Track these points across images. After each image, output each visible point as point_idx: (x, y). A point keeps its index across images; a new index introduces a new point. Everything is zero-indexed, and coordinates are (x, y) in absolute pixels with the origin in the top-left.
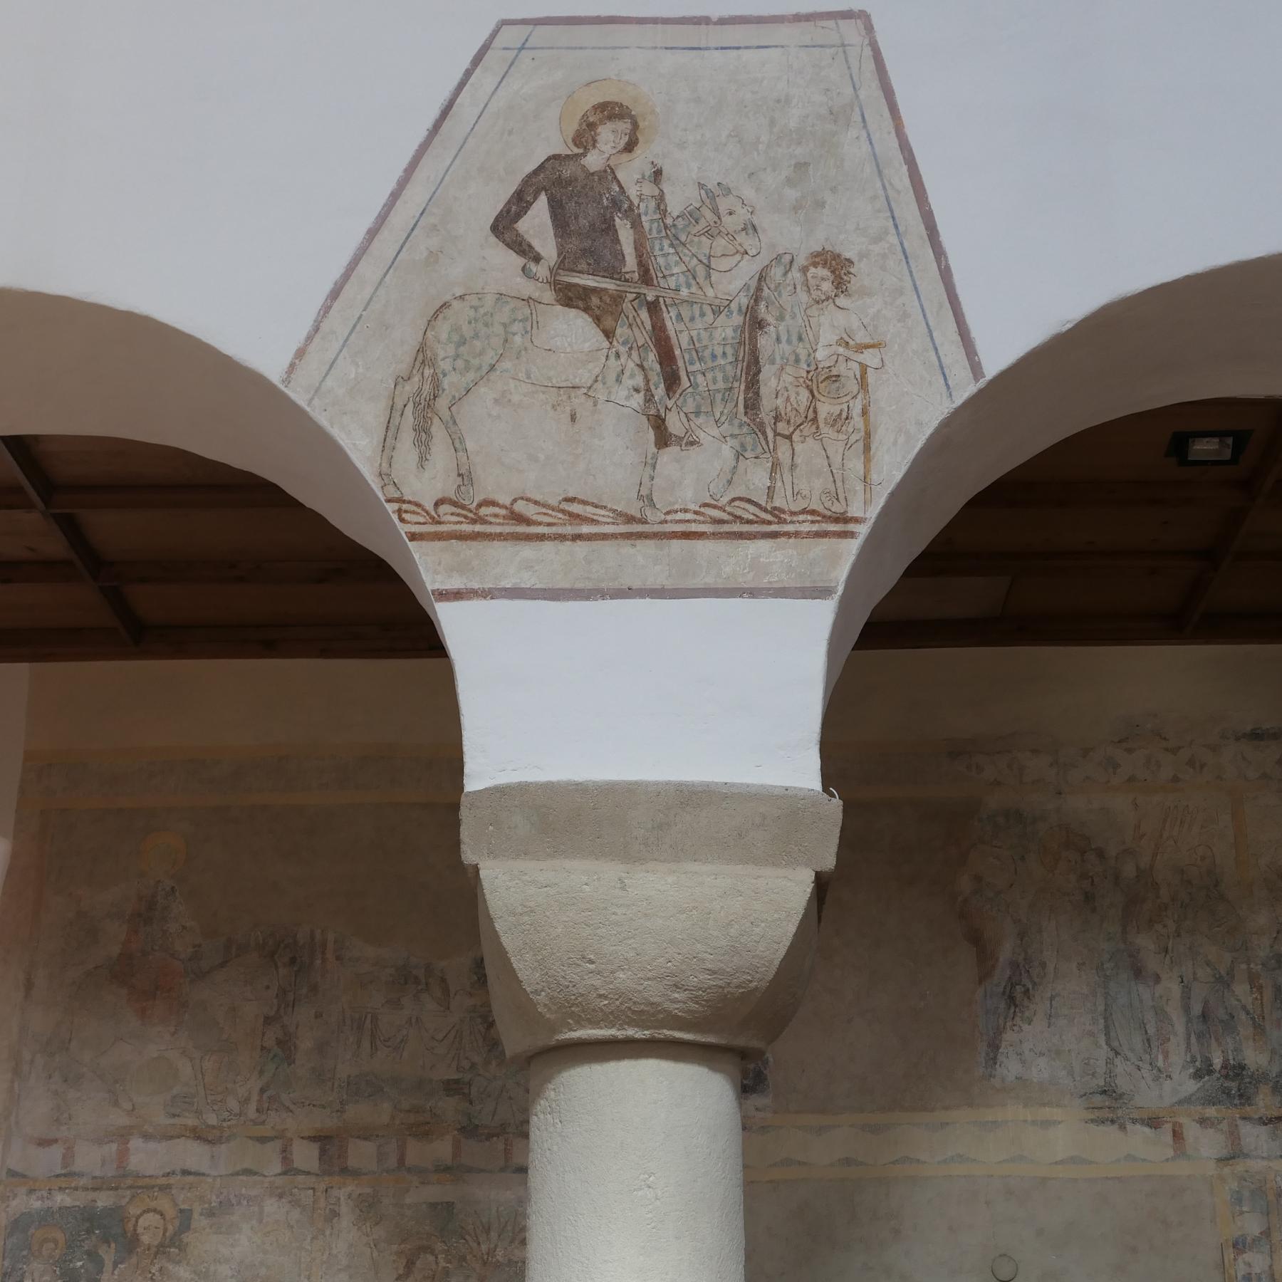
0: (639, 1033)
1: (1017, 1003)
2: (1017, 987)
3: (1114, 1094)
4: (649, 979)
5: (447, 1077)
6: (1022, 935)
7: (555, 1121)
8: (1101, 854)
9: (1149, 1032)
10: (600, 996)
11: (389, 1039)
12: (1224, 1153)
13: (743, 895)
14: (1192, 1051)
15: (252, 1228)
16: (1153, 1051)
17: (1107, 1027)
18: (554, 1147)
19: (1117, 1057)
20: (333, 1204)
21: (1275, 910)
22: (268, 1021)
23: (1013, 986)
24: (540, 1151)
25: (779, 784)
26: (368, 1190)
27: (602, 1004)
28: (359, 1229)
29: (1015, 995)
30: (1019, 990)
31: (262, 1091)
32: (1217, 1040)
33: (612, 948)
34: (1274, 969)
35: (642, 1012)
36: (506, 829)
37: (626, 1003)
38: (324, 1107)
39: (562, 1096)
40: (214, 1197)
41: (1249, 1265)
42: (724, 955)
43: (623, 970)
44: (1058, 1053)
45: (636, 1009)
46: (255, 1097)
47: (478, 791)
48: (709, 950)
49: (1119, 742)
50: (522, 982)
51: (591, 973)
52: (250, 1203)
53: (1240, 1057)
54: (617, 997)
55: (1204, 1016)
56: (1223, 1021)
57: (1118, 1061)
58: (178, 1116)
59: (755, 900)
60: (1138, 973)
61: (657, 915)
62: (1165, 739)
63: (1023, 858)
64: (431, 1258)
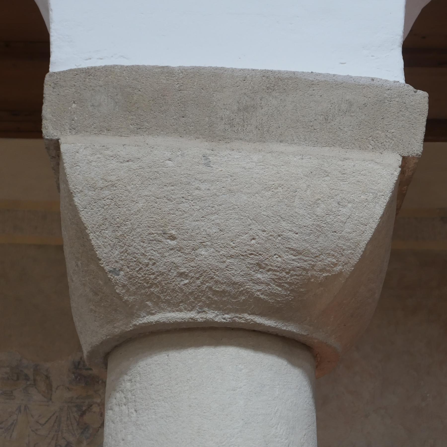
0: (220, 317)
4: (231, 256)
7: (130, 410)
10: (181, 275)
13: (329, 175)
18: (129, 436)
25: (364, 76)
27: (182, 283)
33: (194, 224)
35: (224, 292)
36: (89, 106)
37: (207, 282)
39: (138, 385)
42: (309, 234)
43: (205, 246)
45: (218, 289)
47: (63, 72)
48: (294, 229)
50: (100, 260)
51: (172, 249)
54: (197, 276)
59: (342, 180)
61: (242, 192)
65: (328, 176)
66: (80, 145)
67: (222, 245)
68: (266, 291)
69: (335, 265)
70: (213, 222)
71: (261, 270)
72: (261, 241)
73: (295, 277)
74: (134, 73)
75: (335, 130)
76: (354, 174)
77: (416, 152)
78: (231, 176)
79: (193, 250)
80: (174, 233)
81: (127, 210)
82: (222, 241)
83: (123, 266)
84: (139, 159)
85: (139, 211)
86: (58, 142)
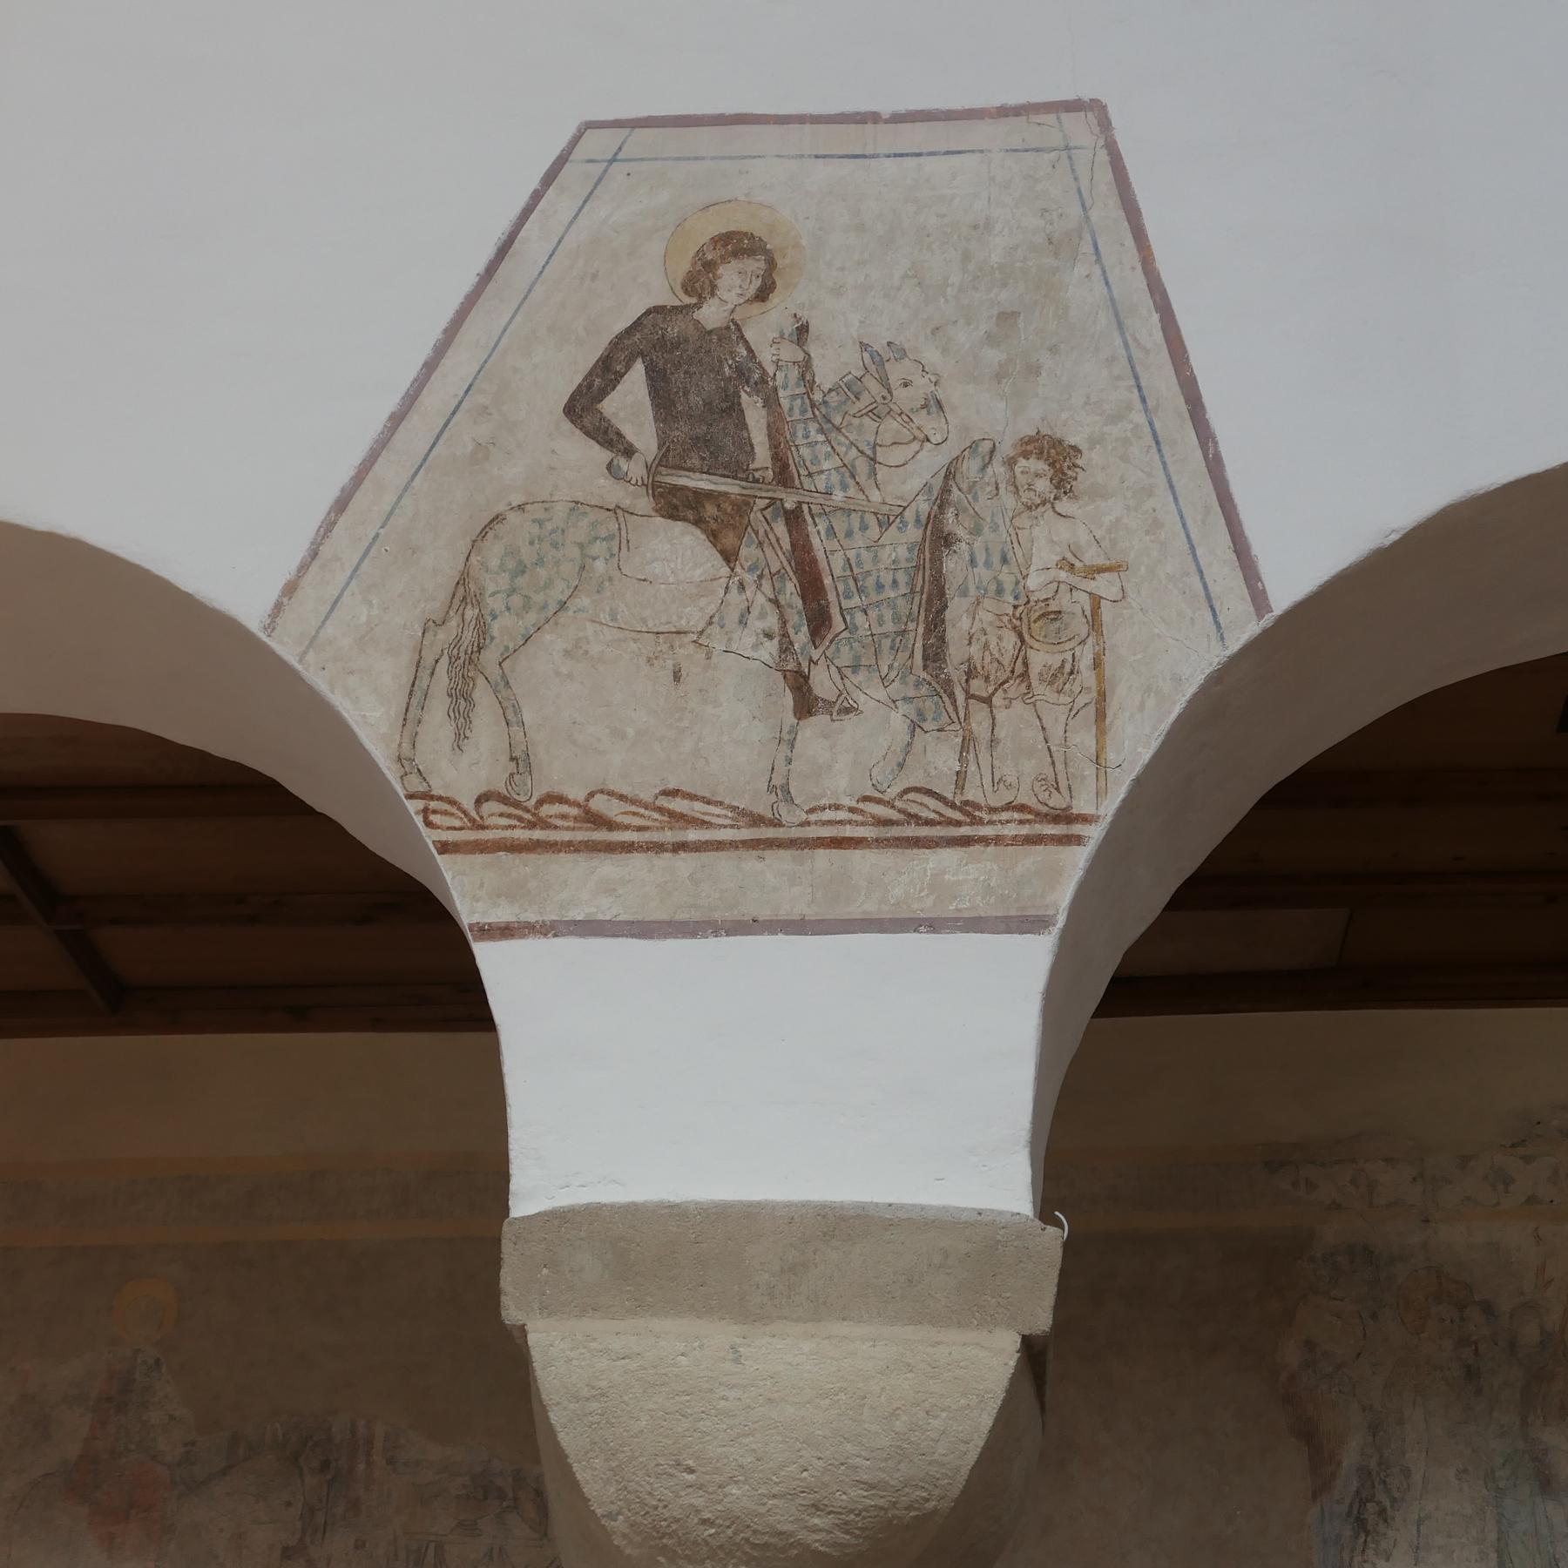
2: (1369, 1505)
4: (774, 1496)
8: (1488, 1309)
10: (704, 1522)
23: (1363, 1503)
29: (1366, 1516)
35: (766, 1545)
37: (742, 1532)
42: (886, 1460)
43: (736, 1482)
48: (863, 1453)
49: (1513, 1146)
50: (589, 1500)
54: (728, 1523)
63: (1374, 1316)
65: (911, 1371)
66: (555, 1333)
67: (760, 1481)
68: (827, 1541)
69: (927, 1500)
70: (746, 1448)
71: (818, 1513)
72: (816, 1474)
73: (870, 1519)
74: (630, 1217)
75: (923, 1298)
76: (949, 1367)
77: (1042, 1328)
78: (772, 1378)
79: (720, 1487)
80: (692, 1465)
81: (624, 1431)
82: (760, 1475)
83: (621, 1508)
84: (639, 1354)
85: (641, 1431)
86: (524, 1330)
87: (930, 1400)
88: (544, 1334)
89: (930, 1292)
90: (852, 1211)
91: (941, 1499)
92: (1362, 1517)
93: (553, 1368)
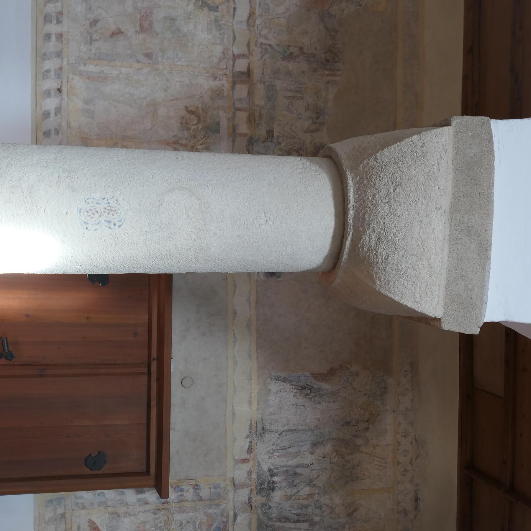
1: (303, 391)
2: (310, 391)
3: (262, 433)
4: (384, 223)
5: (275, 131)
6: (332, 393)
8: (367, 429)
9: (289, 449)
11: (292, 105)
12: (236, 481)
14: (280, 468)
15: (209, 40)
16: (281, 451)
17: (291, 430)
19: (278, 434)
20: (220, 78)
21: (341, 506)
22: (301, 49)
23: (310, 389)
24: (283, 161)
26: (225, 93)
27: (370, 196)
28: (209, 89)
29: (306, 390)
30: (308, 391)
31: (270, 45)
32: (285, 479)
34: (315, 505)
35: (364, 219)
37: (370, 210)
38: (263, 74)
40: (223, 22)
41: (187, 491)
43: (390, 208)
44: (281, 408)
46: (268, 42)
47: (491, 127)
49: (416, 439)
50: (382, 151)
52: (221, 39)
53: (277, 489)
54: (374, 204)
55: (295, 474)
56: (293, 482)
57: (277, 435)
58: (260, 6)
59: (427, 284)
60: (315, 445)
62: (416, 459)
63: (365, 394)
64: (195, 122)
65: (430, 276)
69: (380, 280)
70: (403, 212)
76: (431, 291)
77: (444, 326)
81: (410, 164)
83: (379, 163)
87: (419, 283)
88: (447, 133)
89: (458, 284)
90: (489, 254)
91: (380, 286)
92: (306, 389)
93: (435, 137)
